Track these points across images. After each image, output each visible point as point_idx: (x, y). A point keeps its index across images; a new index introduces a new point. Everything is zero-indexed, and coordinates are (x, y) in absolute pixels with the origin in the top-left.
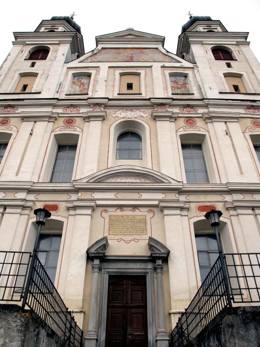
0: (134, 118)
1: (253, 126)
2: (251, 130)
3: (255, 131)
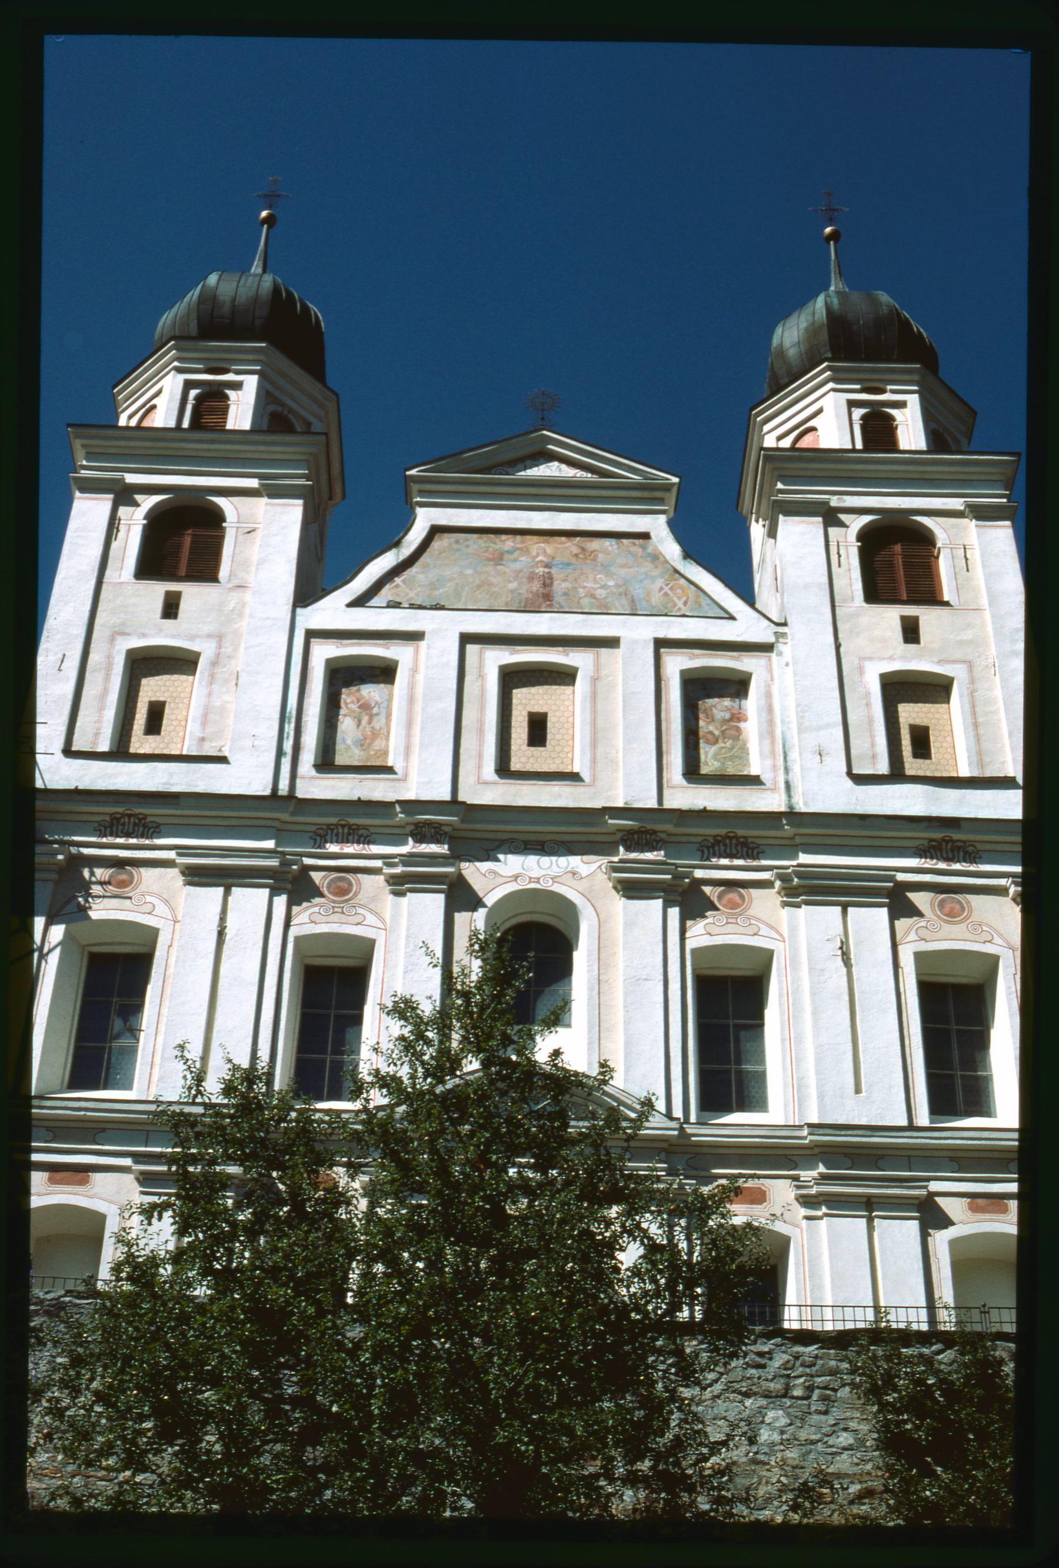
0: (551, 882)
1: (939, 917)
2: (923, 933)
3: (939, 935)
